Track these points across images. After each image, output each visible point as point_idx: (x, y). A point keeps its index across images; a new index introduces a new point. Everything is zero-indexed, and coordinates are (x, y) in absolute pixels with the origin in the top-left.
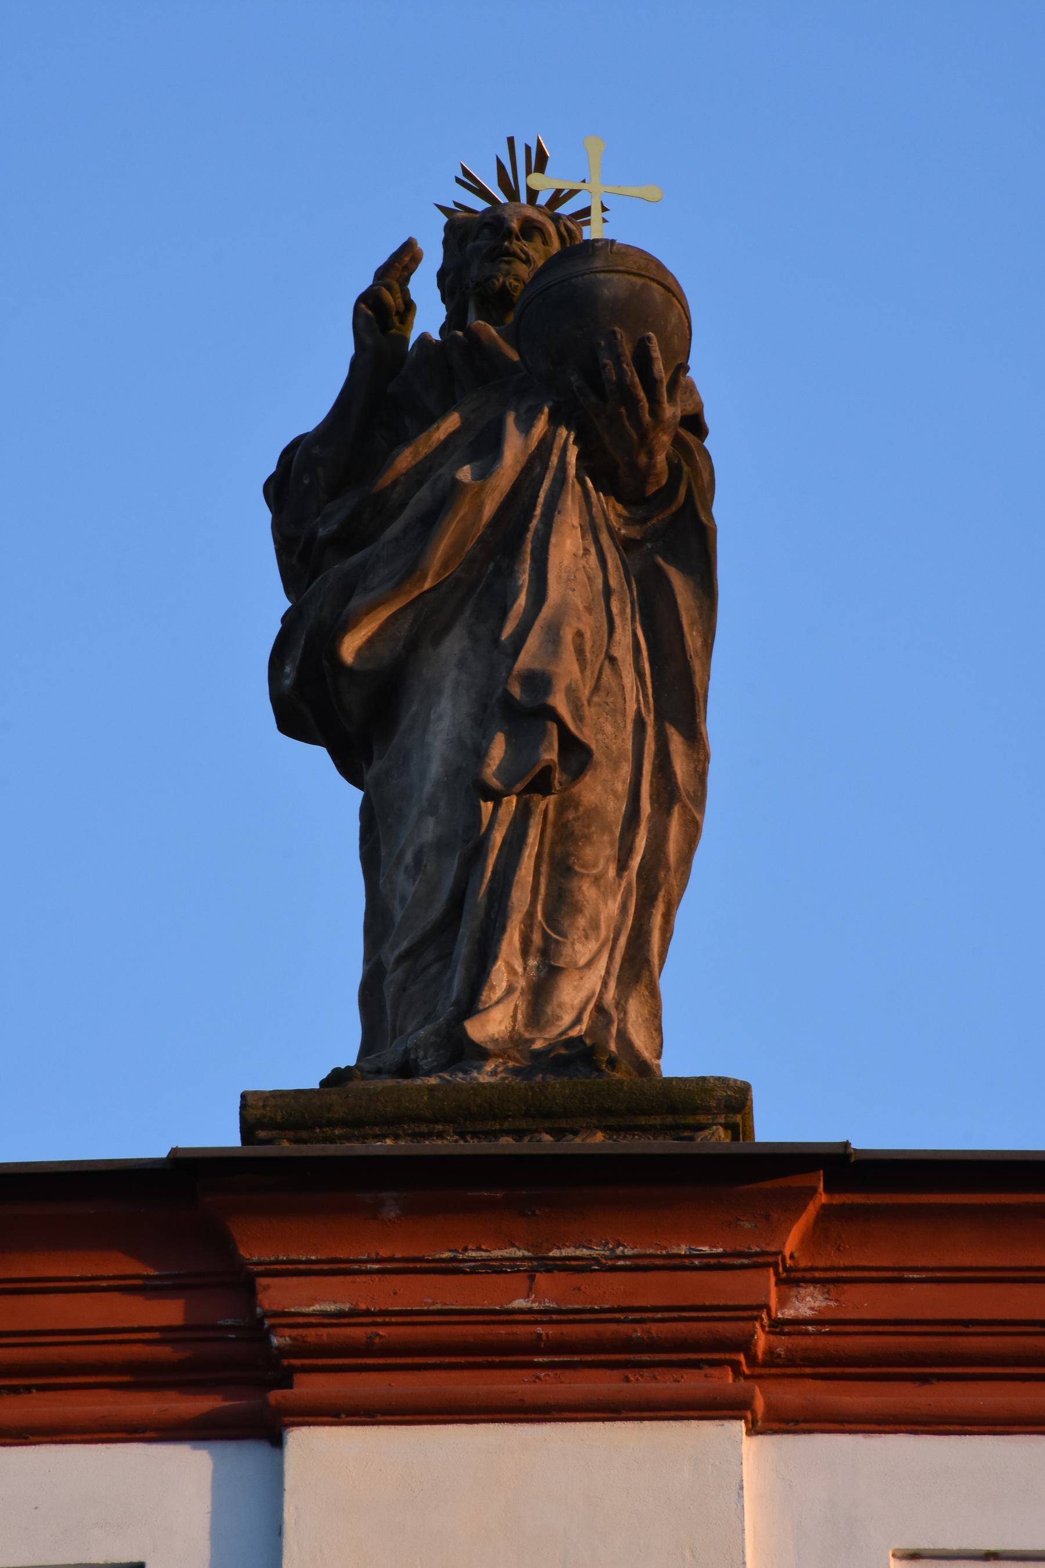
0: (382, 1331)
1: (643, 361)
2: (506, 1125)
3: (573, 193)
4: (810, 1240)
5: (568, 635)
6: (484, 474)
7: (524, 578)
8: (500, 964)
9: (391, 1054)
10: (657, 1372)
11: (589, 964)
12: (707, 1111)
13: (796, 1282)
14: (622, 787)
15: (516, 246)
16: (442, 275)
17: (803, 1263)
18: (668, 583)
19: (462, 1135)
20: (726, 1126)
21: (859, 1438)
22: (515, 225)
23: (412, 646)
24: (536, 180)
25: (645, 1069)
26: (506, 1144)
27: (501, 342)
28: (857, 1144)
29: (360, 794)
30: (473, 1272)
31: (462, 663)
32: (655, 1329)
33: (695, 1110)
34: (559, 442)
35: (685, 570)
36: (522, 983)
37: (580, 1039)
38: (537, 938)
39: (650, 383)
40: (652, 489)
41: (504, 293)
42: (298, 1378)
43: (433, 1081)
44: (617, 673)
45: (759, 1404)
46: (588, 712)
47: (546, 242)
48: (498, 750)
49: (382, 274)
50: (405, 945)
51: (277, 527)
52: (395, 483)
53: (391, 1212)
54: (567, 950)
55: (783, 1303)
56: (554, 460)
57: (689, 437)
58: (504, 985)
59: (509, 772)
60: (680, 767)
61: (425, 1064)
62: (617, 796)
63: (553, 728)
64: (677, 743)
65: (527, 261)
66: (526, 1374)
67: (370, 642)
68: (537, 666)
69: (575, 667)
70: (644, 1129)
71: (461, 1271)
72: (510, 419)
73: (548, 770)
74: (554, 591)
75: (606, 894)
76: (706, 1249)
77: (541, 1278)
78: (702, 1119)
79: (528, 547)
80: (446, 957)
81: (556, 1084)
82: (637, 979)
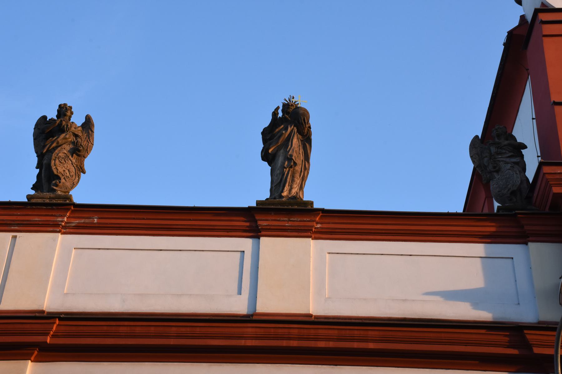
0: (271, 227)
1: (304, 120)
2: (286, 205)
3: (297, 101)
4: (320, 218)
5: (295, 150)
6: (286, 132)
7: (290, 144)
8: (286, 187)
9: (273, 197)
10: (302, 233)
11: (296, 187)
12: (308, 204)
13: (318, 223)
14: (300, 168)
15: (291, 107)
16: (282, 110)
17: (319, 221)
18: (306, 144)
19: (281, 206)
20: (311, 206)
21: (324, 240)
22: (290, 105)
23: (277, 151)
24: (293, 100)
25: (302, 199)
26: (286, 207)
27: (288, 117)
28: (325, 208)
29: (271, 168)
30: (282, 221)
31: (283, 153)
32: (302, 228)
33: (307, 204)
34: (294, 129)
35: (308, 144)
36: (288, 189)
37: (294, 196)
38: (290, 184)
39: (305, 123)
40: (305, 134)
41: (289, 112)
42: (262, 232)
43: (278, 200)
44: (300, 155)
45: (313, 237)
46: (297, 159)
47: (294, 107)
48: (286, 163)
49: (275, 110)
50: (275, 184)
51: (262, 137)
52: (276, 133)
53: (273, 214)
54: (293, 186)
55: (316, 226)
56: (294, 131)
57: (309, 129)
58: (286, 189)
59: (288, 166)
60: (307, 166)
61: (277, 198)
62: (299, 168)
63: (293, 161)
64: (307, 163)
65: (291, 109)
66: (287, 232)
67: (272, 150)
68: (291, 154)
69: (295, 154)
70: (301, 206)
71: (280, 221)
72: (289, 126)
73: (292, 166)
74: (293, 145)
75: (298, 180)
76: (308, 219)
77: (289, 222)
78: (308, 205)
79: (291, 140)
80: (280, 186)
81: (292, 201)
82: (301, 189)
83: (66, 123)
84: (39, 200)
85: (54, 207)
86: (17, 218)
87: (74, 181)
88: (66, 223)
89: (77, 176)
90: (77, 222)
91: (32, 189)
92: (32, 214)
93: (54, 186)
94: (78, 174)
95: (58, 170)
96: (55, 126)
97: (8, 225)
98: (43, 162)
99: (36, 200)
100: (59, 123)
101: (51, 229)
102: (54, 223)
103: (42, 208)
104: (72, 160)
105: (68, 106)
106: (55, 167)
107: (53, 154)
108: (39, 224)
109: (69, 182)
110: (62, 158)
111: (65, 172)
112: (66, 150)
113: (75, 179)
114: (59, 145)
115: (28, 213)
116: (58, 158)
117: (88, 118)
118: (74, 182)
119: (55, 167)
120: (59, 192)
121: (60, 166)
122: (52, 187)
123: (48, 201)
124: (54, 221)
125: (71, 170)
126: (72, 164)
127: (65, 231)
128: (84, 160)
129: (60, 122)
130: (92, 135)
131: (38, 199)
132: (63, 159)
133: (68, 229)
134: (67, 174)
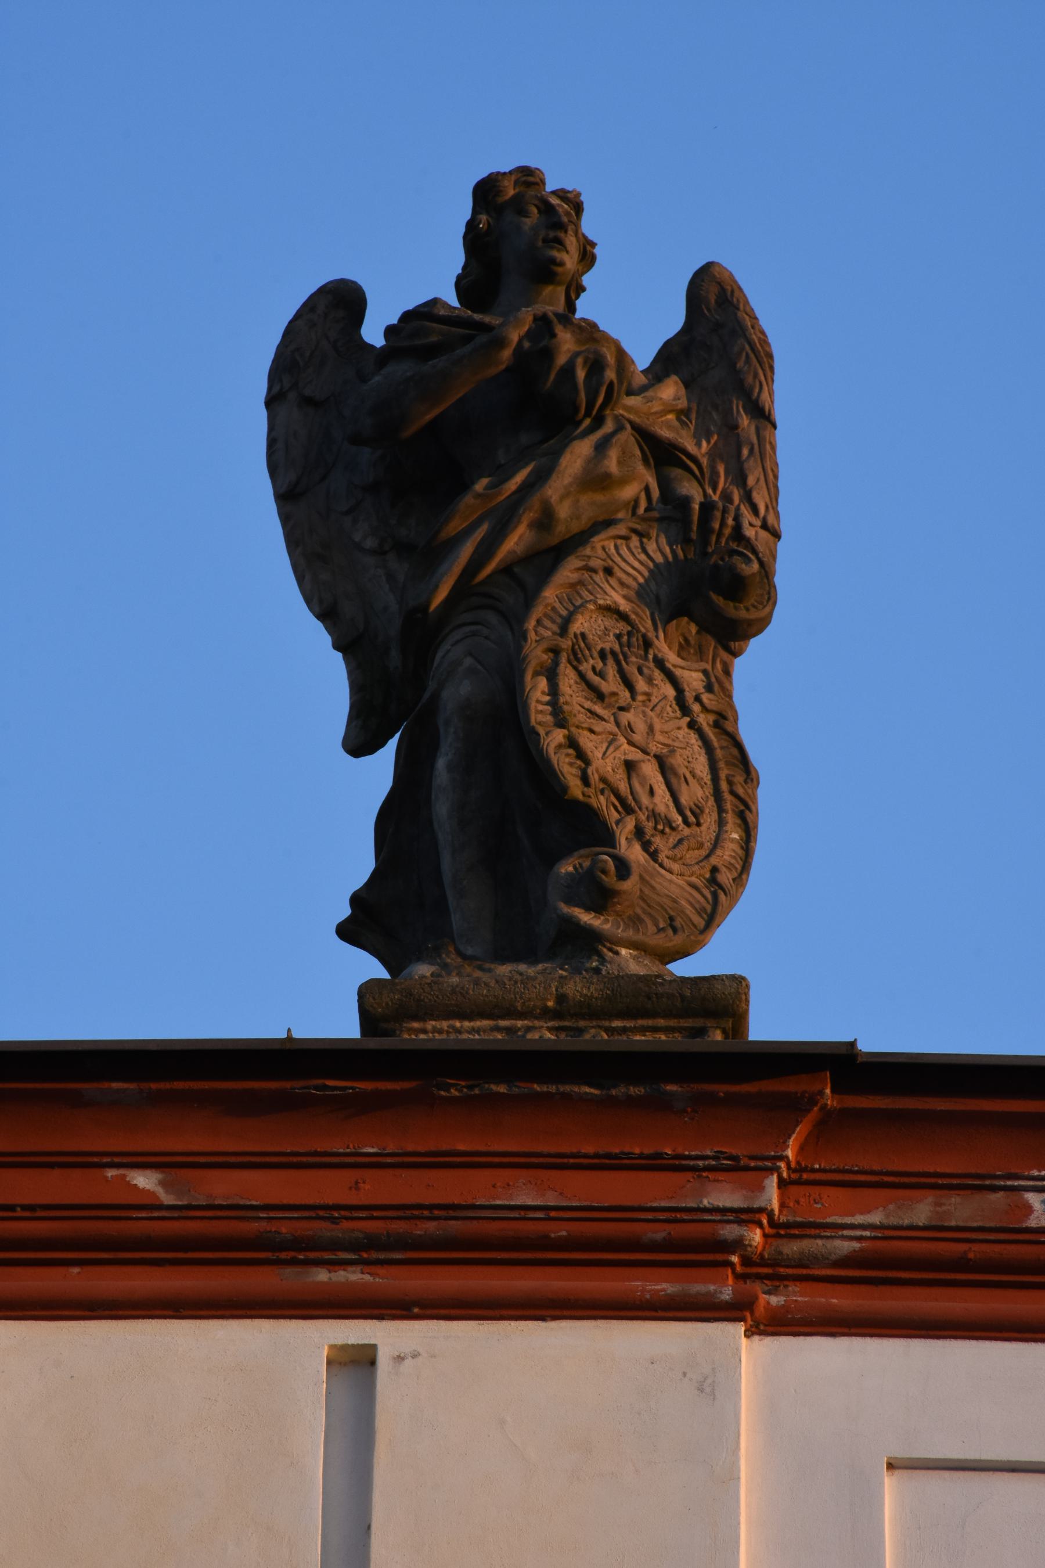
28: (864, 1046)
83: (579, 342)
84: (473, 1031)
85: (671, 1088)
86: (356, 1186)
87: (714, 860)
88: (779, 1230)
89: (730, 818)
90: (876, 1218)
91: (347, 932)
92: (482, 1148)
93: (570, 901)
94: (732, 792)
95: (587, 762)
96: (493, 371)
97: (284, 1255)
98: (435, 697)
99: (444, 1024)
100: (527, 345)
101: (666, 1286)
102: (678, 1231)
103: (566, 1097)
104: (678, 672)
105: (550, 187)
106: (559, 736)
107: (531, 624)
108: (545, 1243)
109: (676, 867)
110: (602, 654)
111: (643, 781)
112: (622, 584)
113: (717, 843)
114: (554, 541)
115: (445, 1147)
116: (576, 659)
117: (712, 295)
118: (714, 870)
119: (559, 736)
120: (624, 952)
121: (599, 727)
122: (565, 909)
123: (548, 1035)
124: (675, 1214)
125: (677, 761)
126: (684, 709)
127: (785, 1308)
128: (727, 672)
129: (529, 335)
130: (764, 451)
131: (463, 1016)
132: (610, 661)
133: (793, 1287)
134: (652, 792)
